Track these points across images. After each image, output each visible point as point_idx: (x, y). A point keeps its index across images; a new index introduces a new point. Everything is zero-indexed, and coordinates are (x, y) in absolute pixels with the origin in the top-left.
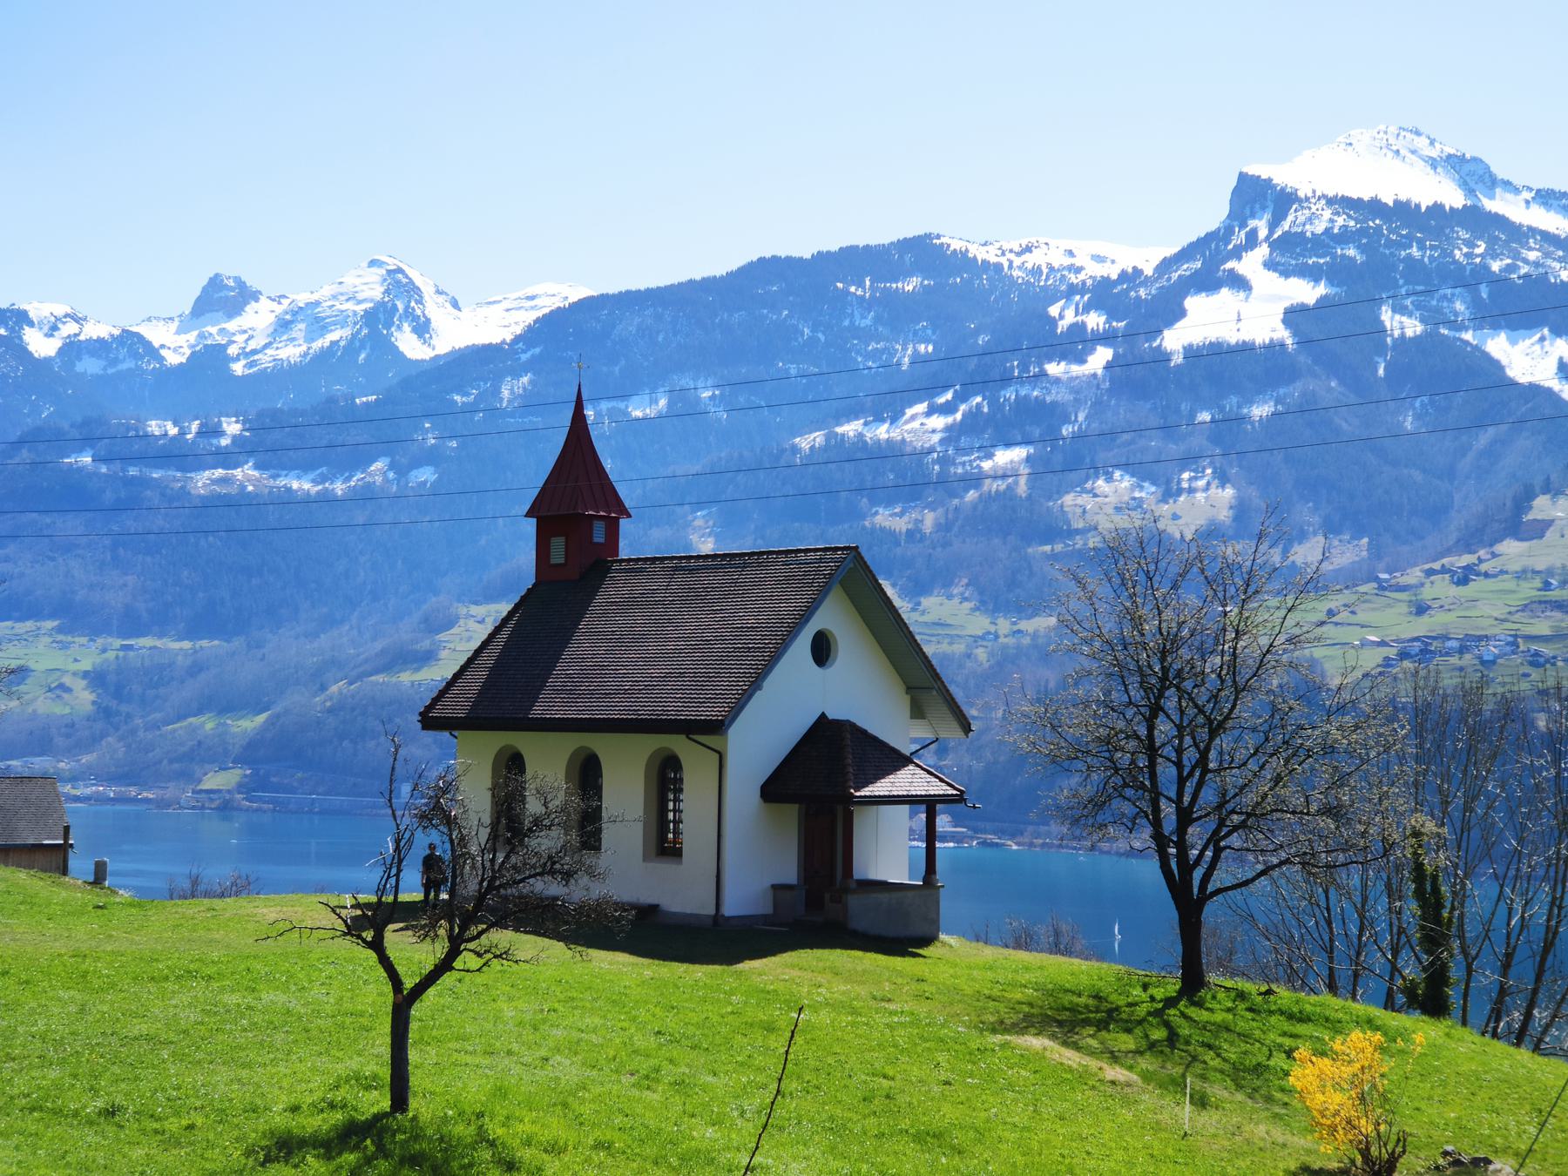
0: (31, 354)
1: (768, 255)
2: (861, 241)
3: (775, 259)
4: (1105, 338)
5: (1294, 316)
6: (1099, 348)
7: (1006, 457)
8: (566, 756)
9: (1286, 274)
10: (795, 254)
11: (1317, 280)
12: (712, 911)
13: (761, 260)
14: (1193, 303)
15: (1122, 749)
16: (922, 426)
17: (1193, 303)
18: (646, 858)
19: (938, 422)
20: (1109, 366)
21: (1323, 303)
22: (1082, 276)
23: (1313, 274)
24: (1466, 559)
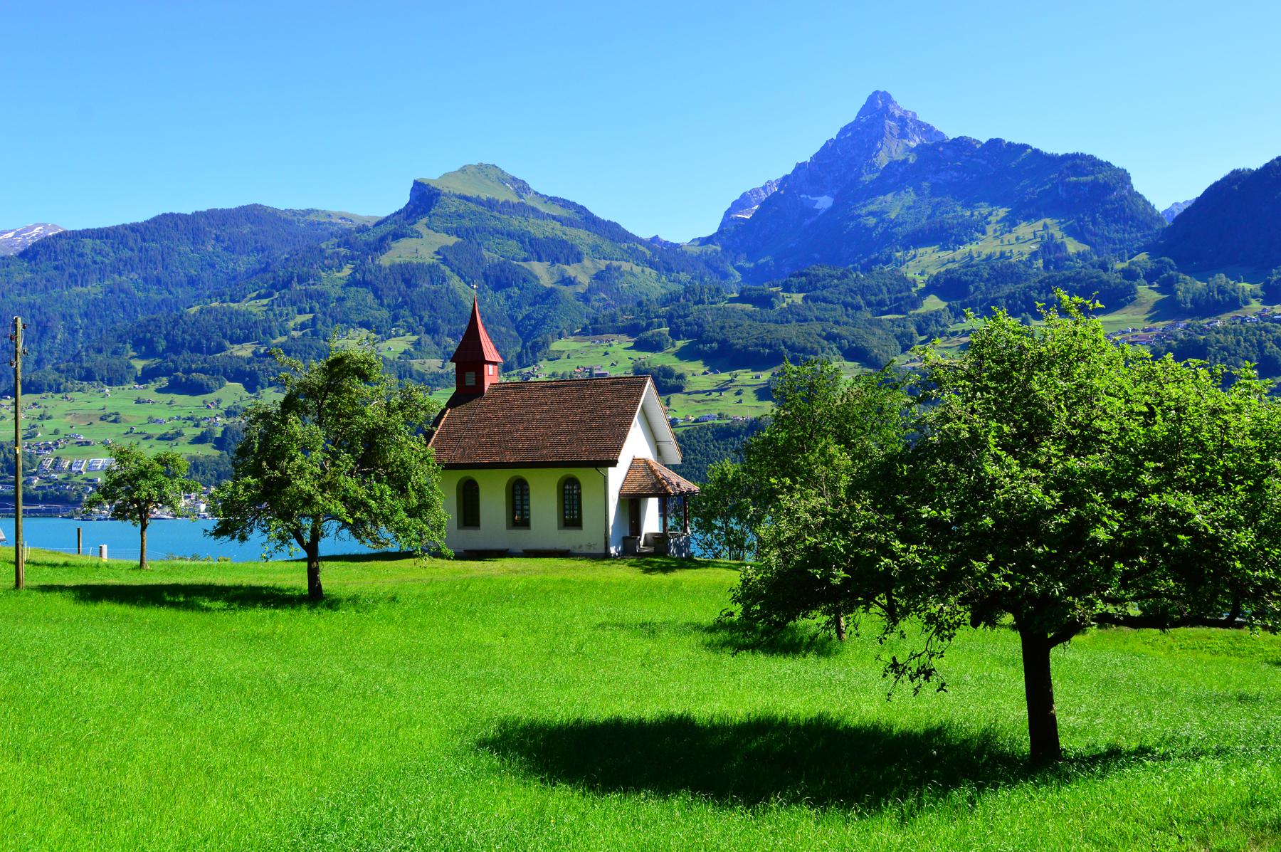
12: (305, 564)
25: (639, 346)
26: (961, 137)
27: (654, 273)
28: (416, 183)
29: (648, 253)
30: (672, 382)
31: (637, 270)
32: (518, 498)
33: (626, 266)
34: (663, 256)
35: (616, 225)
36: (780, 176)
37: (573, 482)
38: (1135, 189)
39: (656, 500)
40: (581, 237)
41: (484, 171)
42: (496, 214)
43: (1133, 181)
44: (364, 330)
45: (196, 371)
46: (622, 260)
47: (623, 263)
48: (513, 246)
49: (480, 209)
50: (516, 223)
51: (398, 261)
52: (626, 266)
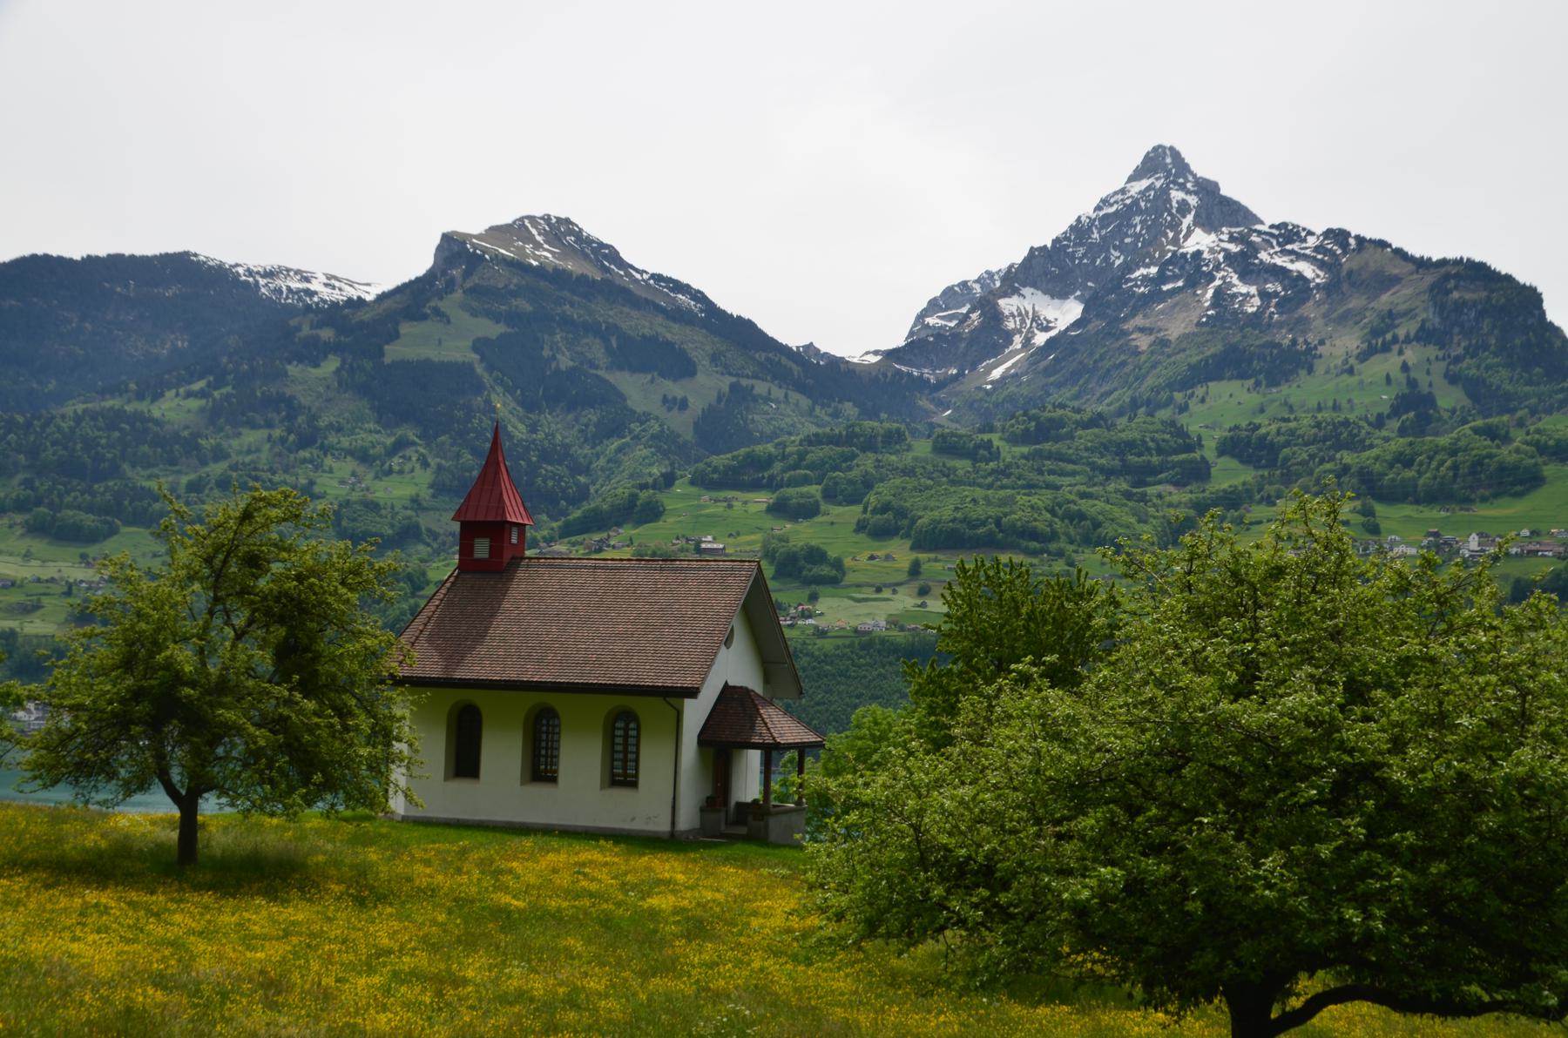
0: (1543, 313)
1: (40, 252)
2: (171, 250)
3: (47, 257)
4: (336, 348)
5: (480, 346)
6: (331, 357)
7: (251, 437)
8: (750, 687)
9: (474, 314)
10: (67, 255)
11: (498, 322)
12: (666, 827)
13: (34, 257)
14: (405, 328)
15: (1455, 679)
16: (174, 409)
17: (405, 328)
18: (522, 783)
19: (194, 404)
20: (338, 371)
21: (502, 336)
22: (316, 299)
23: (497, 318)
24: (597, 537)
25: (779, 509)
26: (186, 254)
27: (805, 402)
28: (447, 238)
29: (796, 369)
30: (825, 570)
31: (778, 393)
32: (619, 740)
33: (761, 388)
34: (815, 374)
35: (749, 325)
36: (1004, 266)
37: (628, 716)
38: (1550, 317)
39: (758, 752)
40: (697, 344)
41: (560, 231)
42: (566, 294)
43: (1546, 305)
44: (870, 454)
45: (70, 507)
46: (756, 376)
47: (756, 382)
48: (596, 350)
49: (543, 284)
50: (605, 312)
51: (688, 347)
52: (761, 388)
